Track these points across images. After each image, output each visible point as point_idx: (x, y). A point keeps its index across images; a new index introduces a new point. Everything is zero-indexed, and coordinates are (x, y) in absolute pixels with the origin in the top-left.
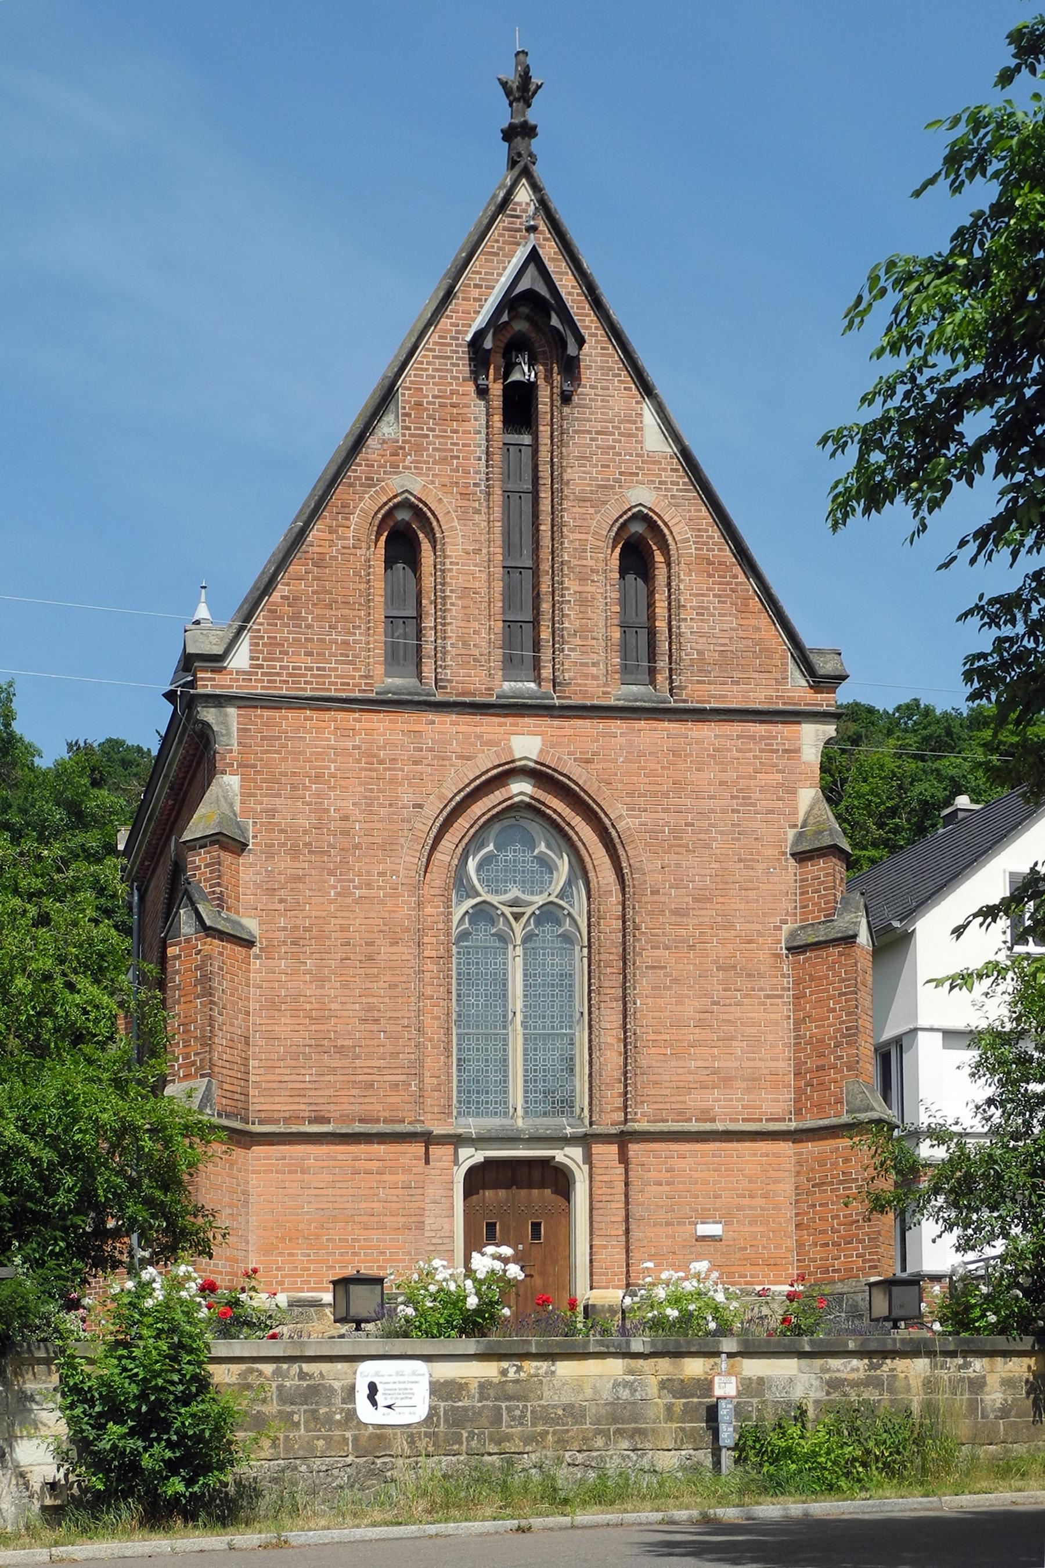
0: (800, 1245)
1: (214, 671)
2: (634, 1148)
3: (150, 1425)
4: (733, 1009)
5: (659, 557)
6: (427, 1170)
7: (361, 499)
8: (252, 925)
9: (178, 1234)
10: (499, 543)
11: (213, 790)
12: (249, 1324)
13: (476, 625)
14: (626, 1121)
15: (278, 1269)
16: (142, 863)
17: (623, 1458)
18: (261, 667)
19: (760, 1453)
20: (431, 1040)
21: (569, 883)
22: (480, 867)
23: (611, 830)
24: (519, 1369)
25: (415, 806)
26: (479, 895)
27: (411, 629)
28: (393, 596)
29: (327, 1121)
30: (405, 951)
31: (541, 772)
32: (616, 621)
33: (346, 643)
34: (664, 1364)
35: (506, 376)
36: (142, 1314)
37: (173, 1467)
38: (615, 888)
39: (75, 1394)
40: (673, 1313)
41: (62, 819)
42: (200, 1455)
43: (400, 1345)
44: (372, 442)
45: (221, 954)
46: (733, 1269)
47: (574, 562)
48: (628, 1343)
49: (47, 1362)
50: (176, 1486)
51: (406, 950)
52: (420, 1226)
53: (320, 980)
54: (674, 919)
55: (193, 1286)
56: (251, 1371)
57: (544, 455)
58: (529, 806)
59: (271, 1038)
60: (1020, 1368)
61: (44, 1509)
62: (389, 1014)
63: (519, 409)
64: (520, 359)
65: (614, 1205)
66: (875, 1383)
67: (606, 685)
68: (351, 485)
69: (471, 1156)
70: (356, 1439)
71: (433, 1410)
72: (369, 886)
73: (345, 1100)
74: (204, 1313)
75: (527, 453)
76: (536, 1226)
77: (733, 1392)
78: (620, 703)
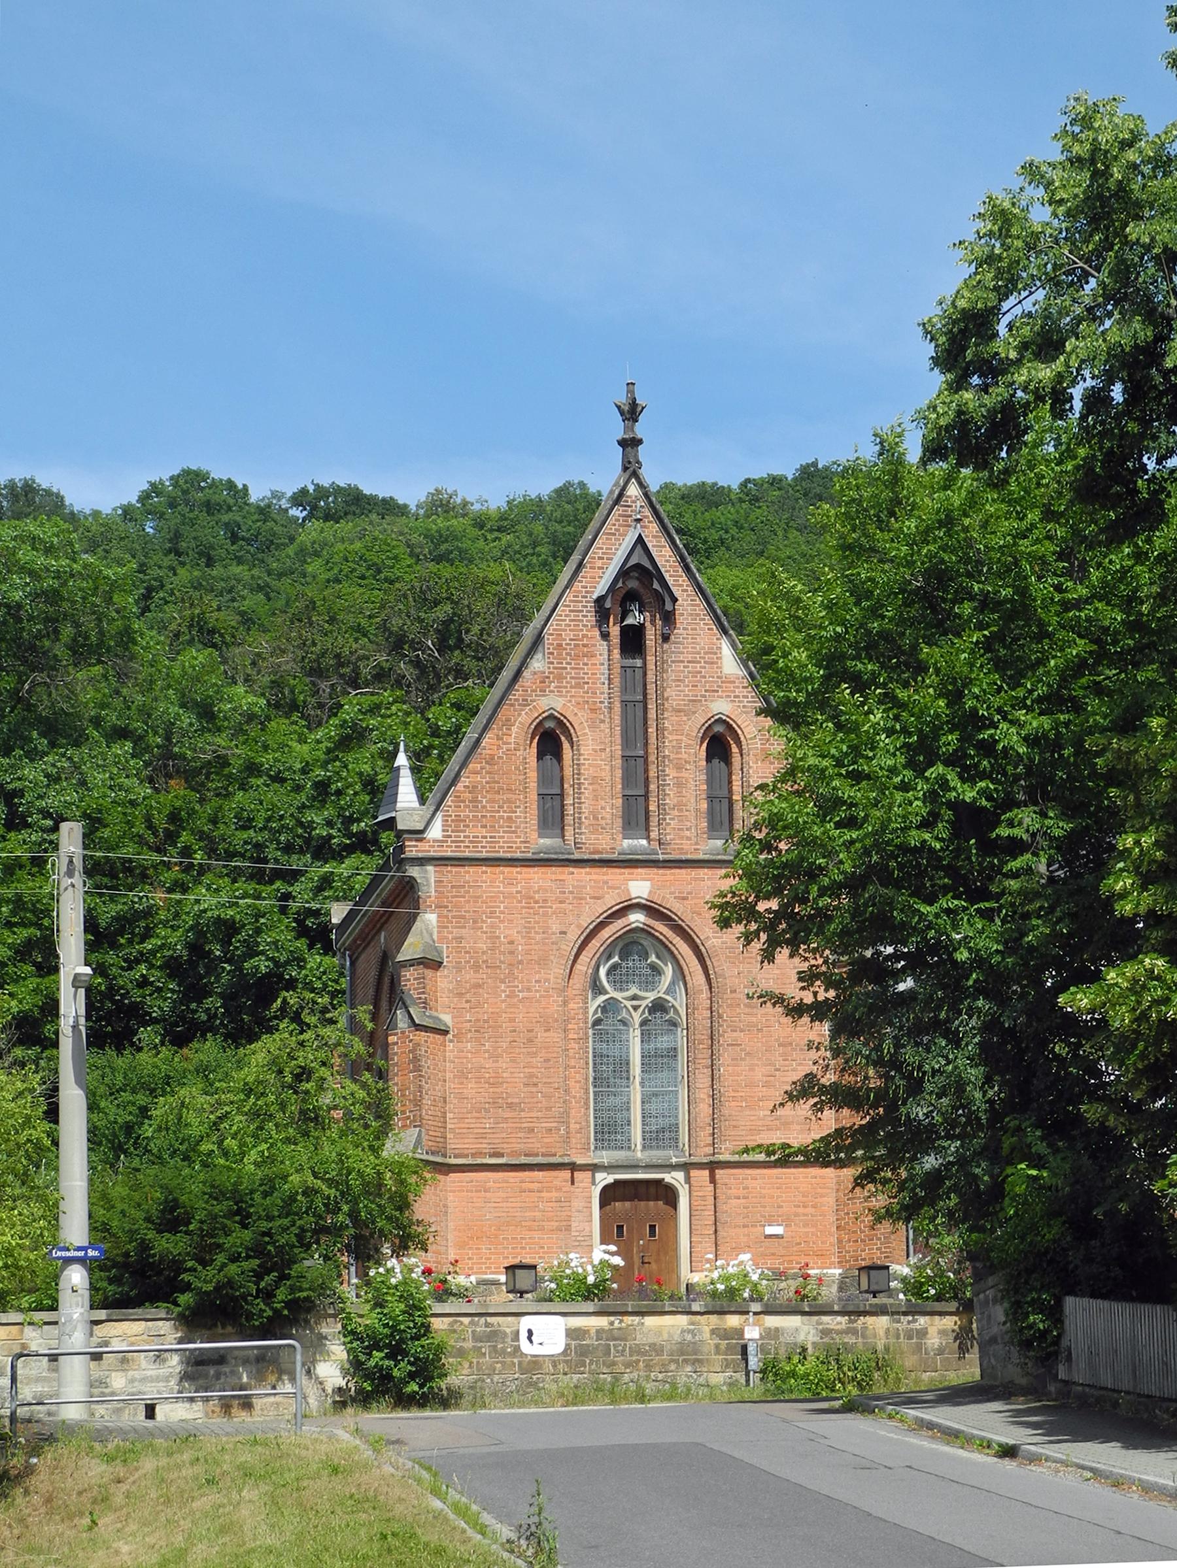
0: (840, 1241)
1: (417, 840)
2: (719, 1173)
3: (396, 1352)
4: (789, 1073)
5: (735, 749)
6: (572, 1189)
7: (519, 715)
8: (447, 1019)
9: (407, 1239)
10: (619, 741)
11: (418, 925)
12: (455, 1295)
13: (603, 803)
14: (714, 1154)
15: (469, 1259)
16: (355, 941)
17: (688, 1377)
18: (450, 836)
19: (776, 1375)
20: (575, 1097)
21: (673, 983)
22: (608, 974)
23: (701, 947)
24: (621, 1321)
25: (561, 933)
26: (606, 993)
27: (557, 803)
28: (543, 779)
29: (501, 1155)
30: (555, 1036)
31: (650, 907)
32: (704, 796)
33: (510, 818)
34: (714, 1318)
35: (622, 622)
36: (389, 1288)
37: (412, 1376)
38: (705, 987)
39: (351, 1334)
40: (721, 1287)
41: (191, 725)
42: (426, 1370)
44: (526, 674)
45: (426, 1041)
46: (791, 1258)
47: (672, 756)
48: (690, 1306)
49: (335, 1316)
50: (413, 1387)
51: (556, 1035)
52: (568, 1228)
53: (495, 1057)
54: (747, 1010)
55: (419, 1270)
56: (456, 1322)
57: (651, 677)
58: (642, 929)
60: (950, 1323)
61: (335, 1402)
62: (544, 1080)
63: (633, 642)
64: (632, 607)
65: (707, 1213)
66: (854, 1332)
67: (697, 844)
68: (512, 705)
69: (605, 1179)
70: (520, 1363)
71: (568, 1346)
72: (529, 990)
73: (514, 1140)
74: (426, 1287)
75: (639, 673)
76: (652, 1227)
77: (757, 1336)
78: (706, 857)
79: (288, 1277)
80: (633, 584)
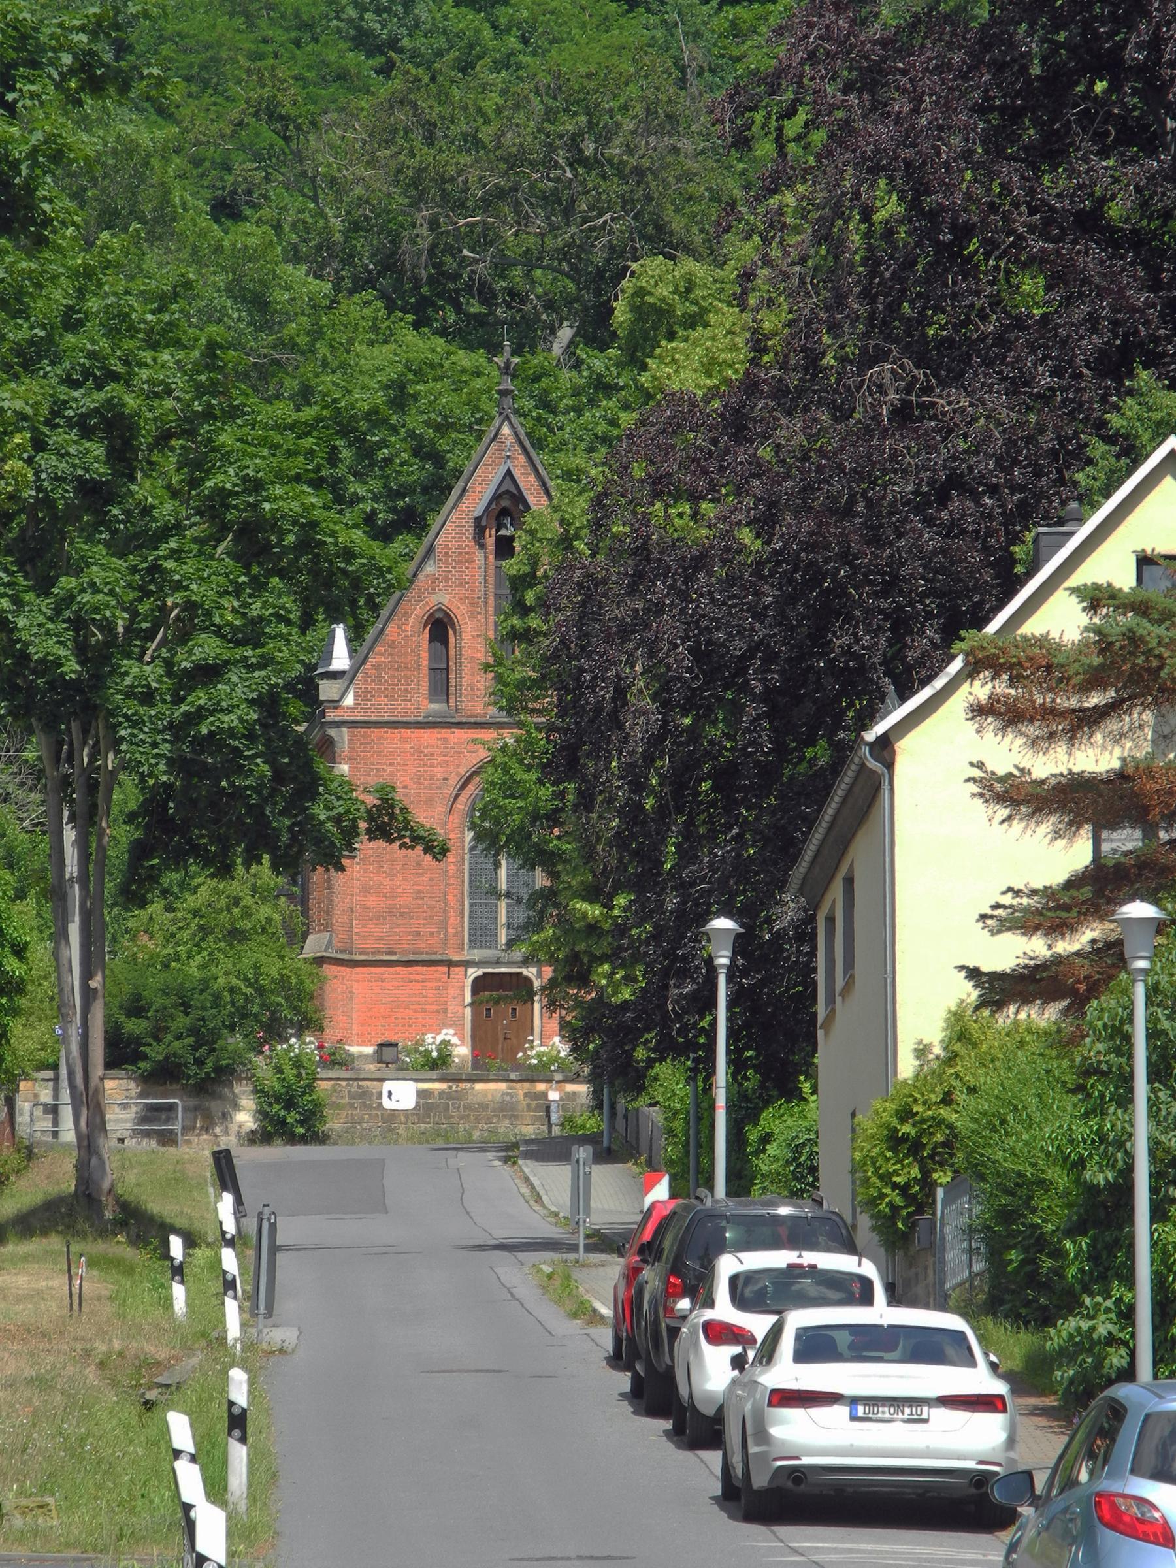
3: (289, 1104)
9: (308, 1023)
12: (340, 1064)
28: (433, 657)
34: (526, 1085)
43: (402, 1074)
44: (421, 576)
52: (445, 1011)
53: (392, 876)
59: (365, 908)
69: (474, 973)
79: (214, 1050)
80: (505, 503)
